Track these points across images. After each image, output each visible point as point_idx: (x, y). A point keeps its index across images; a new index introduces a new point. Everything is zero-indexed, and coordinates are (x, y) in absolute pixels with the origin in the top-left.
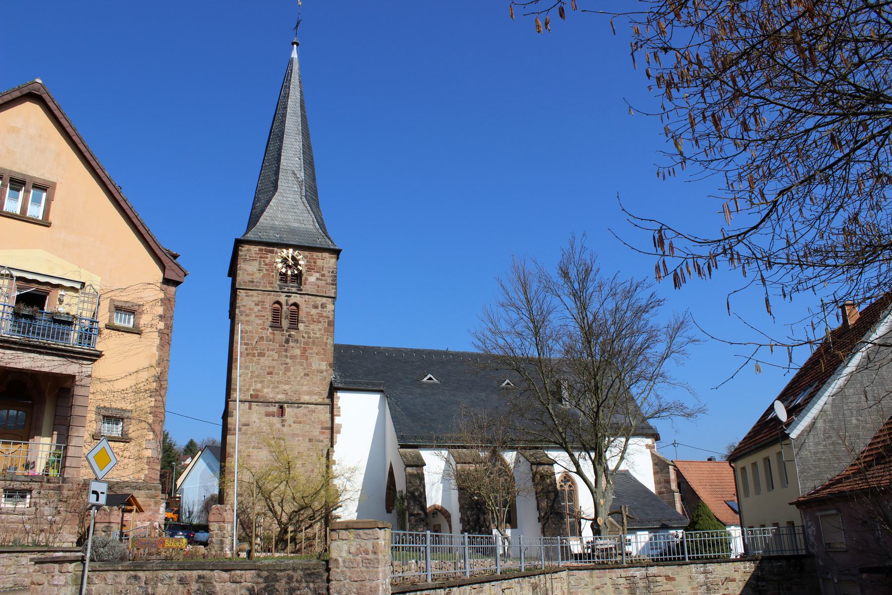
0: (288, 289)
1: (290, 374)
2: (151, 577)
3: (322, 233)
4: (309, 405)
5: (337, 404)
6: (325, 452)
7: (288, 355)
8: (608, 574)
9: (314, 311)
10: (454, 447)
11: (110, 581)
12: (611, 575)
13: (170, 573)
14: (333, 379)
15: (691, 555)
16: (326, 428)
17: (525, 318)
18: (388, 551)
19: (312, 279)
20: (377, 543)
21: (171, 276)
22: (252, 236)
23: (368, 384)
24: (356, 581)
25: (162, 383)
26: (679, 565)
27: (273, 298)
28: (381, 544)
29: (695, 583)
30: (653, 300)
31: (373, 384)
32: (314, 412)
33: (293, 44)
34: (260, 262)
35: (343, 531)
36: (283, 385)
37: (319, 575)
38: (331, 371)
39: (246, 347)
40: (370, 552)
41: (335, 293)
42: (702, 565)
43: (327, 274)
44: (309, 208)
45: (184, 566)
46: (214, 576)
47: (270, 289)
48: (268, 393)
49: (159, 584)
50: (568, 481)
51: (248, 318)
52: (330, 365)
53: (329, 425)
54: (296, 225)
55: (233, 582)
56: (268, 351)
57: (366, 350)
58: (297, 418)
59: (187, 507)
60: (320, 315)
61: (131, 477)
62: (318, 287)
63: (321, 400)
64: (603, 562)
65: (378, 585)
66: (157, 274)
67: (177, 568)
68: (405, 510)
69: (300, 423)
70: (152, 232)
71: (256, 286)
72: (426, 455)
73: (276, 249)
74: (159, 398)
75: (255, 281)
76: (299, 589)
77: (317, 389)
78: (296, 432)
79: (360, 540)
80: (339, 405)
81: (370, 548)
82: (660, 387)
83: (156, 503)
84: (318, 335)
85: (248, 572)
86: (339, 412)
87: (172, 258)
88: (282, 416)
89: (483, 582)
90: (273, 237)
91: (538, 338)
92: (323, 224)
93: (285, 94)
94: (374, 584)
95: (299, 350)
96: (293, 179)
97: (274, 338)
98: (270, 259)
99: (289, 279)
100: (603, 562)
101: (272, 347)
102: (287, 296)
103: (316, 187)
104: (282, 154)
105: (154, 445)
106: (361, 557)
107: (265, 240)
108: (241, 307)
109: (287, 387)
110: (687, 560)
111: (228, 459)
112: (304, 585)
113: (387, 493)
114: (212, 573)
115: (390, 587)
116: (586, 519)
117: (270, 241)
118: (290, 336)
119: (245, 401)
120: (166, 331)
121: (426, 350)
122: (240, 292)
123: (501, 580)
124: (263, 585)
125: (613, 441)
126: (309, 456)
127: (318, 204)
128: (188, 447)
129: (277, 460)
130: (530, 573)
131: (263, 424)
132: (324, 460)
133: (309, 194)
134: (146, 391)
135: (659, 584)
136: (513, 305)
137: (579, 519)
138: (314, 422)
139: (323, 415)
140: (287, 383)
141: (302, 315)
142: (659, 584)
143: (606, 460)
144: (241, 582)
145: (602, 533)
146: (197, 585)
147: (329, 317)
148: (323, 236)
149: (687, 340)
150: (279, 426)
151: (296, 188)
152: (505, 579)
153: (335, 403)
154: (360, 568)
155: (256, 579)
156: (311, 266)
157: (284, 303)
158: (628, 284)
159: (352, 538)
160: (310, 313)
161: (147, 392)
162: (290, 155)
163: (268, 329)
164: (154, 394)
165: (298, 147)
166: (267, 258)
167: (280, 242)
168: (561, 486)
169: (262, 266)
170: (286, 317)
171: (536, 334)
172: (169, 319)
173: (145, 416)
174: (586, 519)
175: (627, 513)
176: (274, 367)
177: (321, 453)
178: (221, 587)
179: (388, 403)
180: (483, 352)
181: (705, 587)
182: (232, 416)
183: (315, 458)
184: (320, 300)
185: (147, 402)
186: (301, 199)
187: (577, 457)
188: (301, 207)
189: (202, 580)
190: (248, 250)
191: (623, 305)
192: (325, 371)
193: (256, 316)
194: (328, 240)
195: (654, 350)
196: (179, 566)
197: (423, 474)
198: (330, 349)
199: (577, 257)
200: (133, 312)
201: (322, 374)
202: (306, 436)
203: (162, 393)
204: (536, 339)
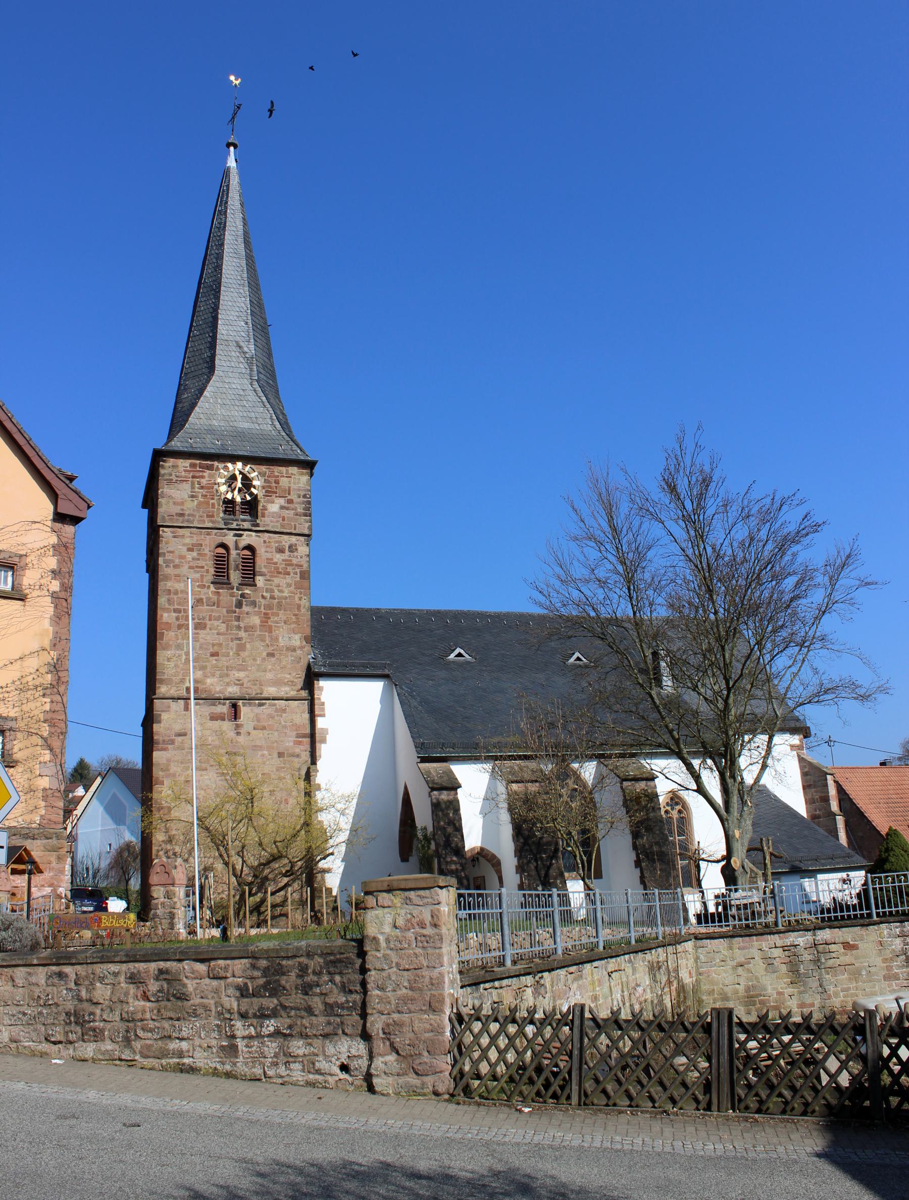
0: (237, 525)
1: (247, 653)
2: (84, 974)
3: (286, 437)
4: (276, 701)
5: (319, 699)
6: (303, 772)
7: (242, 625)
8: (755, 942)
9: (278, 557)
10: (501, 758)
11: (20, 982)
12: (760, 945)
13: (114, 968)
14: (311, 660)
15: (881, 910)
16: (304, 736)
17: (610, 557)
18: (454, 921)
19: (272, 508)
20: (439, 910)
21: (66, 508)
22: (179, 444)
23: (365, 666)
24: (408, 970)
25: (60, 674)
26: (862, 925)
27: (214, 538)
28: (444, 911)
29: (888, 952)
30: (806, 524)
31: (374, 667)
32: (284, 711)
33: (229, 145)
34: (193, 483)
35: (385, 894)
36: (235, 672)
37: (349, 963)
38: (308, 648)
39: (177, 614)
40: (428, 924)
41: (310, 528)
42: (898, 924)
43: (296, 500)
44: (264, 399)
45: (135, 955)
46: (184, 969)
47: (210, 525)
48: (214, 684)
49: (98, 984)
50: (677, 804)
51: (177, 571)
52: (306, 639)
53: (308, 731)
54: (246, 425)
55: (214, 978)
56: (210, 620)
57: (359, 613)
58: (258, 721)
59: (90, 863)
60: (289, 563)
61: (20, 819)
62: (284, 520)
63: (295, 693)
64: (747, 926)
65: (441, 975)
66: (46, 507)
67: (124, 959)
68: (432, 857)
69: (264, 728)
70: (35, 441)
71: (188, 521)
72: (461, 771)
73: (216, 464)
74: (58, 698)
75: (187, 513)
76: (318, 985)
77: (288, 676)
78: (258, 743)
79: (411, 907)
80: (322, 700)
81: (427, 918)
82: (819, 657)
83: (60, 859)
84: (286, 594)
85: (237, 962)
86: (323, 710)
87: (68, 482)
88: (236, 718)
89: (582, 963)
90: (211, 445)
91: (632, 587)
92: (287, 423)
93: (220, 223)
94: (435, 973)
95: (257, 617)
96: (238, 354)
97: (219, 601)
98: (207, 479)
99: (238, 508)
100: (747, 926)
101: (217, 615)
102: (236, 535)
103: (272, 366)
104: (220, 316)
105: (52, 769)
106: (413, 933)
107: (199, 450)
108: (167, 554)
109: (241, 675)
110: (875, 918)
111: (156, 788)
112: (326, 978)
113: (400, 831)
114: (180, 965)
115: (458, 977)
116: (708, 861)
117: (208, 451)
118: (243, 596)
119: (179, 699)
120: (63, 595)
121: (450, 611)
122: (163, 531)
123: (607, 958)
124: (261, 981)
125: (749, 742)
126: (280, 779)
127: (277, 392)
128: (76, 770)
129: (233, 787)
130: (645, 946)
131: (208, 732)
132: (302, 784)
133: (262, 376)
134: (36, 687)
135: (833, 955)
136: (592, 537)
137: (695, 860)
138: (285, 727)
139: (298, 715)
140: (242, 668)
141: (261, 563)
142: (833, 955)
143: (740, 770)
144: (226, 978)
145: (740, 882)
146: (157, 983)
147: (302, 566)
148: (287, 442)
149: (858, 583)
150: (232, 734)
151: (243, 367)
152: (612, 957)
153: (316, 696)
154: (413, 949)
155: (249, 973)
156: (270, 487)
157: (231, 545)
158: (768, 501)
159: (399, 905)
160: (272, 559)
161: (39, 689)
162: (231, 317)
163: (209, 587)
164: (48, 692)
165: (243, 305)
166: (203, 477)
167: (222, 452)
168: (667, 812)
169: (197, 490)
170: (237, 568)
171: (629, 582)
172: (67, 575)
173: (36, 726)
174: (708, 861)
175: (771, 850)
176: (220, 645)
177: (297, 773)
178: (195, 985)
179: (398, 695)
180: (546, 612)
181: (904, 957)
182: (160, 722)
183: (289, 781)
184: (287, 540)
185: (39, 704)
186: (251, 385)
187: (697, 767)
188: (252, 397)
189: (164, 976)
190: (173, 466)
191: (761, 533)
192: (300, 648)
193: (190, 568)
194: (295, 447)
195: (809, 600)
196: (127, 955)
197: (457, 801)
198: (306, 615)
199: (688, 463)
200: (11, 567)
201: (294, 653)
202: (273, 748)
203: (62, 689)
204: (629, 589)
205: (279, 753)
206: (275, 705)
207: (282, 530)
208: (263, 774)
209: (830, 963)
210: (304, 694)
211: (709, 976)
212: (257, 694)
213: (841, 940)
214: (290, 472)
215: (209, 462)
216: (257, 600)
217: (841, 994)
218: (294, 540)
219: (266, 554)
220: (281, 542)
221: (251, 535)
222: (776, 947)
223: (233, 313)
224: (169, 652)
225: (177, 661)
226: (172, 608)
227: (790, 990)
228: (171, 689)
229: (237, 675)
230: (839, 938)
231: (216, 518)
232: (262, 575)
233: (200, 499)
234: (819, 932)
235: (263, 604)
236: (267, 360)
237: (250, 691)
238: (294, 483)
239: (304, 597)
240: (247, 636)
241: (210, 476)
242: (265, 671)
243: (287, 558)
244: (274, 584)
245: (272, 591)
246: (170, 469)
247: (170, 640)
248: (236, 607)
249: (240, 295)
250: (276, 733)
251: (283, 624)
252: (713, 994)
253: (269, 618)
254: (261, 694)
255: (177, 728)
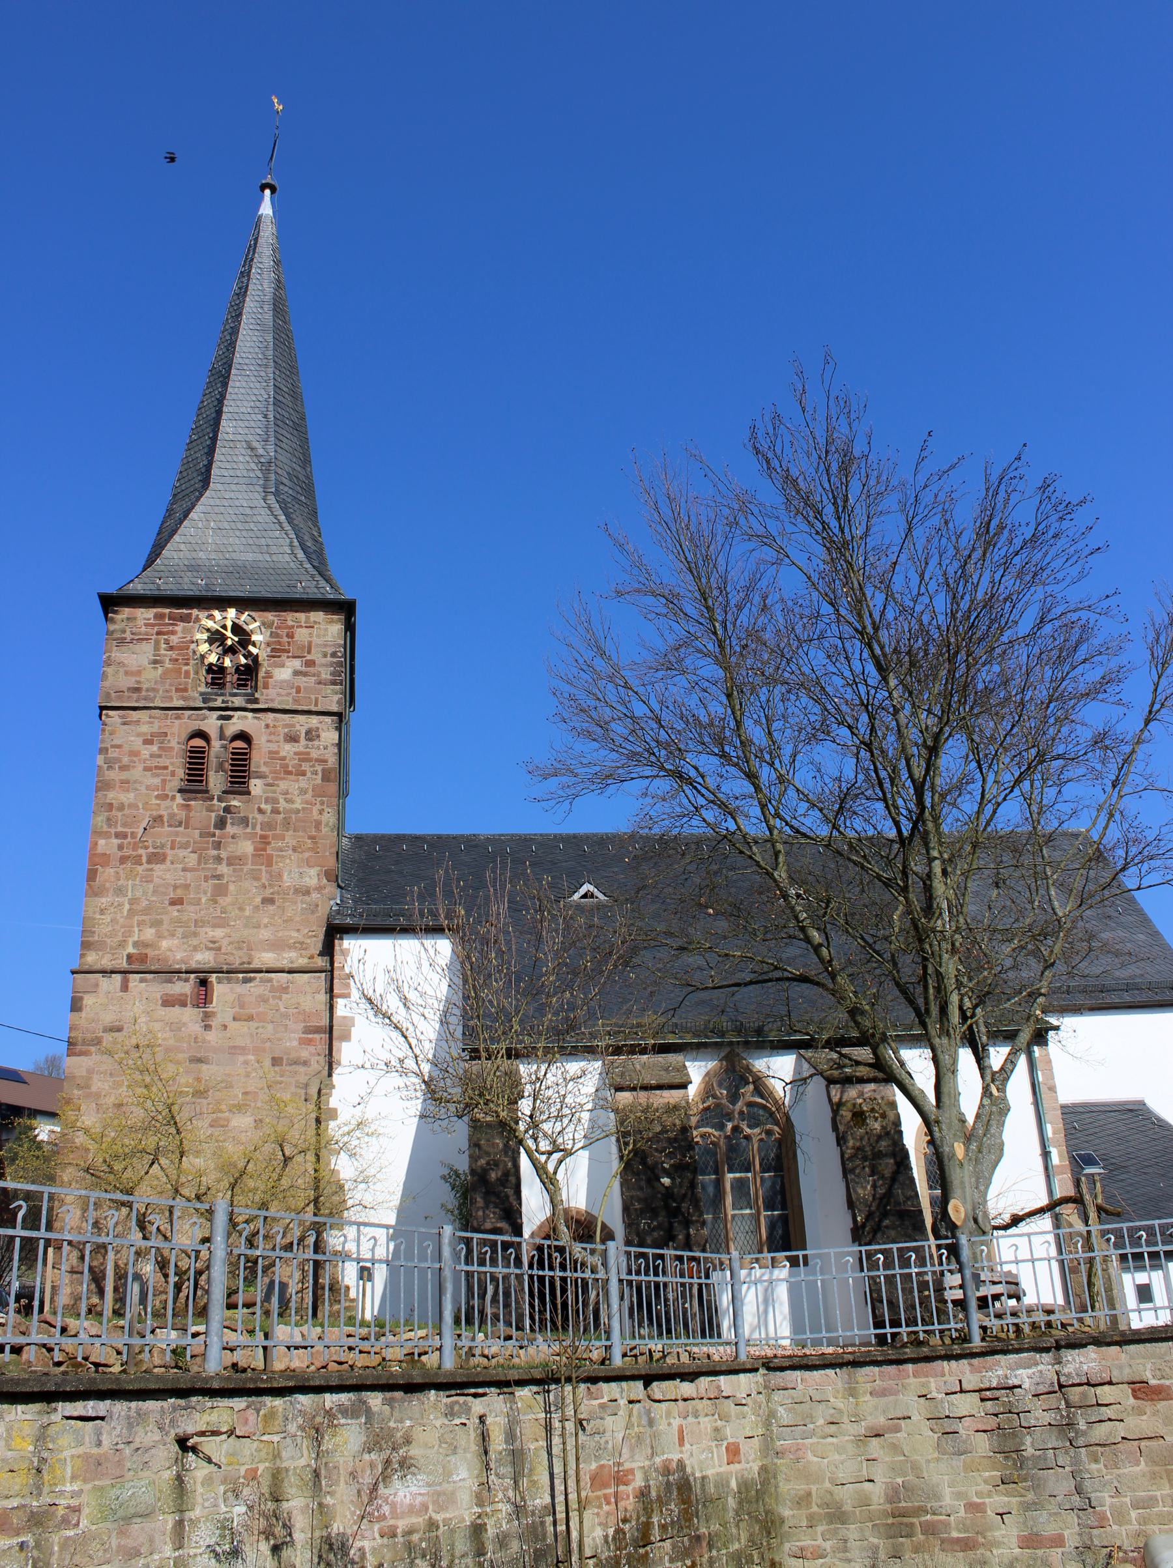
0: (223, 702)
1: (229, 899)
4: (273, 975)
7: (224, 854)
9: (288, 749)
16: (317, 1030)
22: (139, 587)
32: (285, 990)
33: (263, 187)
34: (157, 643)
36: (208, 930)
38: (331, 889)
39: (119, 841)
44: (283, 518)
47: (180, 703)
51: (124, 775)
54: (250, 557)
56: (172, 848)
58: (242, 1006)
62: (298, 691)
63: (306, 961)
69: (250, 1018)
73: (195, 612)
75: (145, 686)
77: (295, 934)
78: (239, 1042)
84: (298, 806)
95: (249, 843)
96: (248, 458)
97: (188, 818)
109: (219, 933)
118: (227, 810)
119: (113, 972)
127: (314, 513)
131: (157, 1026)
138: (286, 1016)
139: (309, 997)
141: (259, 759)
147: (326, 761)
148: (312, 576)
150: (196, 1028)
156: (279, 643)
157: (213, 733)
162: (243, 410)
163: (173, 798)
166: (173, 633)
169: (163, 652)
170: (220, 767)
176: (186, 887)
184: (302, 723)
186: (265, 500)
188: (264, 516)
190: (128, 619)
192: (316, 889)
193: (146, 769)
194: (323, 583)
201: (306, 898)
202: (264, 1050)
205: (273, 1059)
206: (270, 980)
207: (294, 707)
208: (245, 1093)
209: (1101, 1432)
210: (321, 962)
211: (798, 1460)
212: (243, 963)
213: (1127, 1375)
214: (312, 619)
215: (185, 611)
216: (251, 816)
217: (1134, 1514)
218: (315, 721)
219: (269, 745)
220: (293, 726)
221: (246, 717)
222: (962, 1391)
223: (245, 403)
224: (104, 900)
225: (115, 913)
226: (113, 831)
227: (999, 1500)
228: (102, 957)
229: (211, 934)
230: (1121, 1368)
231: (190, 693)
232: (260, 776)
233: (168, 665)
234: (1069, 1355)
235: (259, 821)
236: (299, 468)
237: (230, 959)
238: (318, 636)
239: (327, 810)
240: (231, 872)
241: (184, 630)
242: (259, 927)
243: (302, 749)
244: (278, 790)
245: (275, 801)
246: (124, 624)
247: (106, 881)
248: (216, 827)
249: (260, 379)
250: (270, 1027)
251: (290, 852)
252: (809, 1505)
253: (269, 843)
254: (249, 963)
255: (108, 1018)
